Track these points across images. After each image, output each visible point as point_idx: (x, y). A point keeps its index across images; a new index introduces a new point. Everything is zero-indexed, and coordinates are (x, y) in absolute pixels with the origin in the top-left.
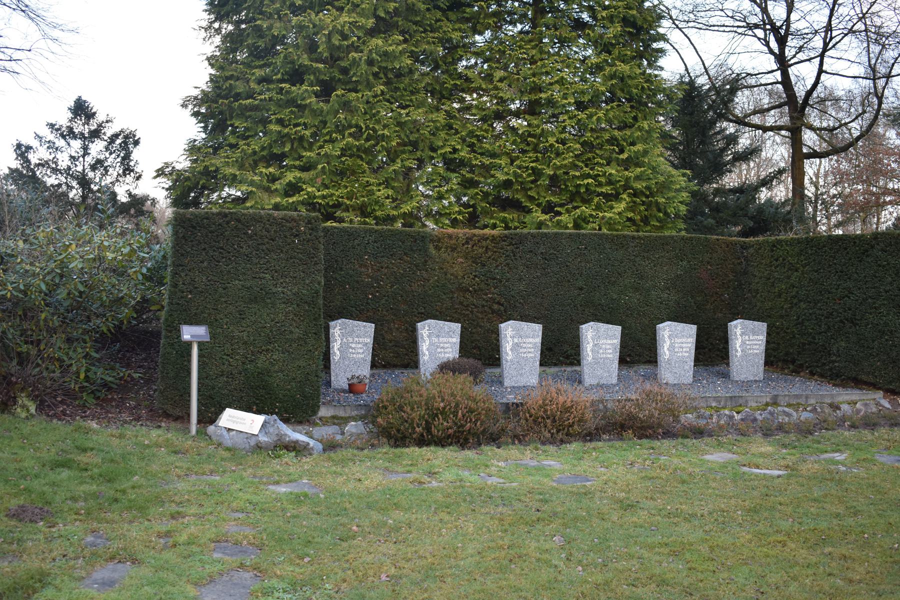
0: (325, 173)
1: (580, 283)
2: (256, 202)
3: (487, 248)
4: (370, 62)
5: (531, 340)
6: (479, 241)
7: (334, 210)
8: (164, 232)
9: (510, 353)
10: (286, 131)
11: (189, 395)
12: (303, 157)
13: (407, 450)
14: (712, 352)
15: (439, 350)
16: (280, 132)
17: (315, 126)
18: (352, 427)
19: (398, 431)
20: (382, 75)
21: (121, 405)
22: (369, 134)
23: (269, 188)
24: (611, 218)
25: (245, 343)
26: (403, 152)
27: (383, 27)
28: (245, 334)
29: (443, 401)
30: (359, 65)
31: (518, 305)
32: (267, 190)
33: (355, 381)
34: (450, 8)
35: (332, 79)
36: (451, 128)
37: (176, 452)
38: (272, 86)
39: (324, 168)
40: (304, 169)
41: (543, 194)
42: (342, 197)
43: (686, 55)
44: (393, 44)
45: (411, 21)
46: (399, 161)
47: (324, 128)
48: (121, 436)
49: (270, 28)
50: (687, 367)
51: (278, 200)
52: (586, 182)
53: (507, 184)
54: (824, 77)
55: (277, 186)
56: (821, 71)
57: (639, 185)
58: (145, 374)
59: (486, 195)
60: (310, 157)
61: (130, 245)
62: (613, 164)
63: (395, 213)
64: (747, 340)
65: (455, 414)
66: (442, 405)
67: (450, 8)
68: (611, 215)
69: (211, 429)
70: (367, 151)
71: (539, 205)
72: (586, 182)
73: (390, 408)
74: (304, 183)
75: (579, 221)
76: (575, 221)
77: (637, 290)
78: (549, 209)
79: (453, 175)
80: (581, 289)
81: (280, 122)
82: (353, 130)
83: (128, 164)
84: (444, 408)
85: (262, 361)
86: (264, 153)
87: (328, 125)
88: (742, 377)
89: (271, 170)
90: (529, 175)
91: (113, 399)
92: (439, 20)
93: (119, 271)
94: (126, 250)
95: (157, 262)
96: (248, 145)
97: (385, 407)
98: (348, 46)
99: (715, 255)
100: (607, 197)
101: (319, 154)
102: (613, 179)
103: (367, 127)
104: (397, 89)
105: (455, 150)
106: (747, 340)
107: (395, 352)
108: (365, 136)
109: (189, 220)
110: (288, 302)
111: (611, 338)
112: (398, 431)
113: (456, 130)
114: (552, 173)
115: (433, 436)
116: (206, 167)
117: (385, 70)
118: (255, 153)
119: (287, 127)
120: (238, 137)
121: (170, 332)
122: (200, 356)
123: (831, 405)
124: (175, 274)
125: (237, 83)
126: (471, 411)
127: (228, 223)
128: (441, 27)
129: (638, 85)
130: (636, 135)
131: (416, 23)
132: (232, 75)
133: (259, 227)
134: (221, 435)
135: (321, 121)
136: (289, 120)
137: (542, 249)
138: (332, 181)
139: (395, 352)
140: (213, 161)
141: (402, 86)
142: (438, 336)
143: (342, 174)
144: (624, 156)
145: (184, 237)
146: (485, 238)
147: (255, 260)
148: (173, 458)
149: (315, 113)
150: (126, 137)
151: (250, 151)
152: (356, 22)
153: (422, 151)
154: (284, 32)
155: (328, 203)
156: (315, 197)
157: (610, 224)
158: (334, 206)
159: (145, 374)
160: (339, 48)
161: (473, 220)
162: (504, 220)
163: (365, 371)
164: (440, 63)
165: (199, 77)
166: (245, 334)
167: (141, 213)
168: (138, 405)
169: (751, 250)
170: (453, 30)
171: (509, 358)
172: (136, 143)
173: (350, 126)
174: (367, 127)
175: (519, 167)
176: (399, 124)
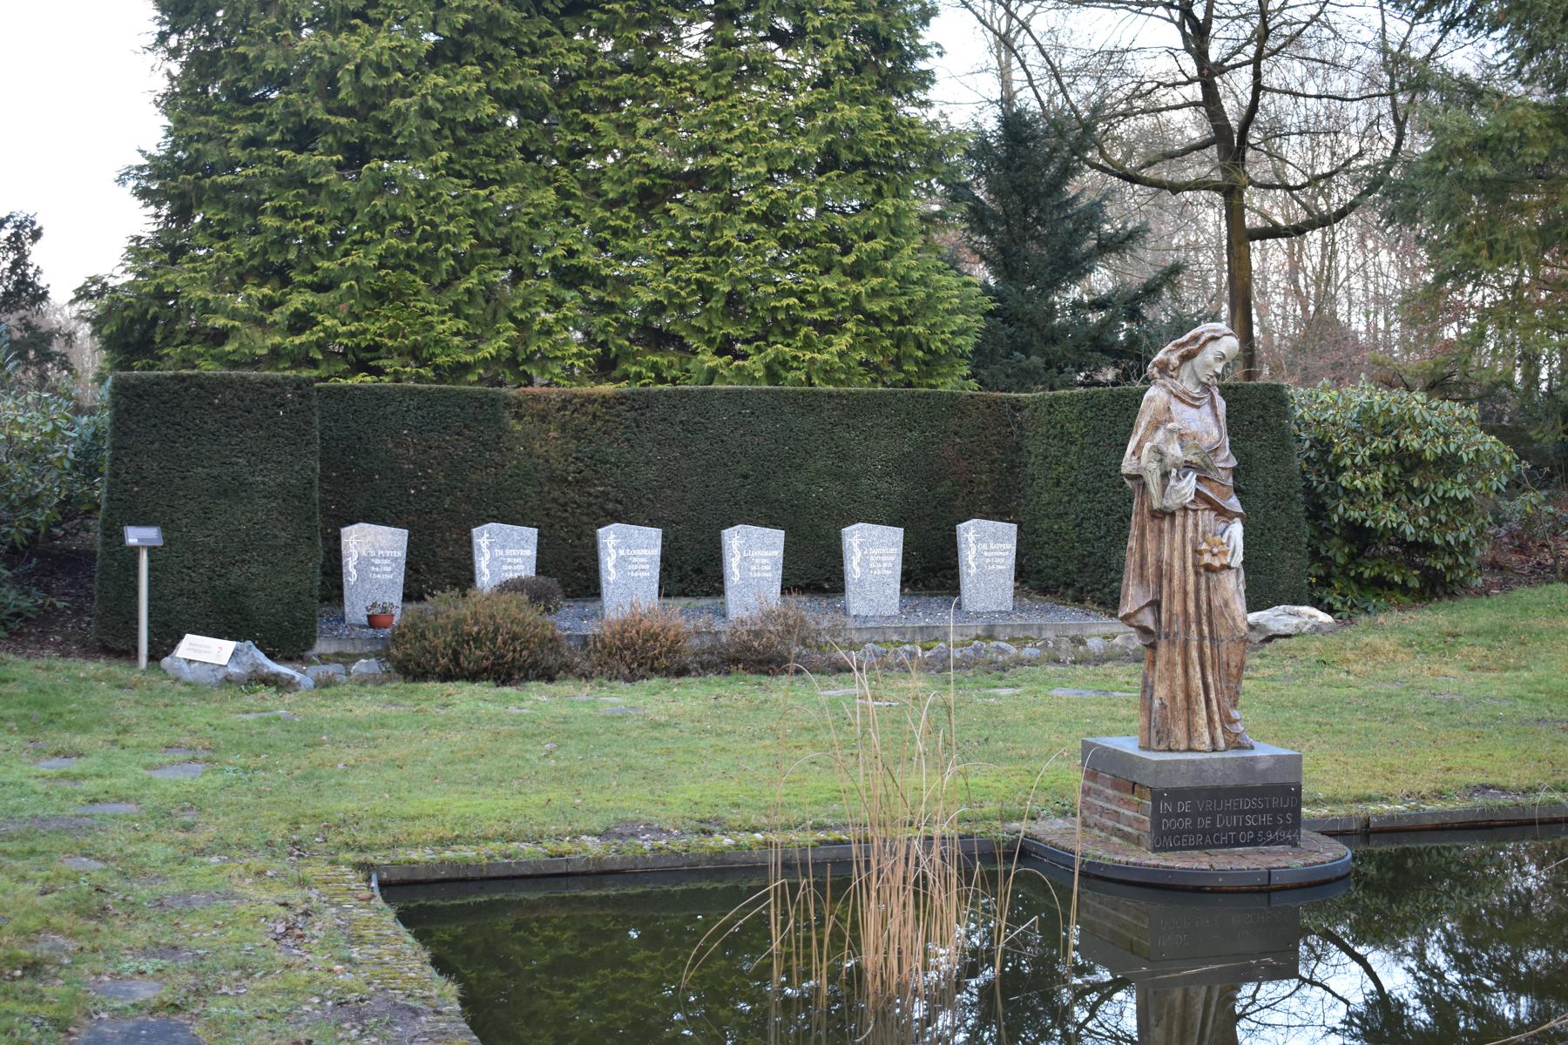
0: (353, 296)
1: (745, 468)
2: (242, 344)
3: (594, 416)
4: (426, 113)
5: (645, 552)
6: (582, 405)
7: (369, 355)
8: (95, 394)
9: (613, 571)
10: (289, 226)
11: (137, 621)
12: (317, 268)
13: (424, 685)
14: (930, 571)
15: (505, 567)
16: (279, 229)
17: (336, 218)
18: (361, 666)
19: (418, 665)
20: (447, 132)
21: (42, 642)
22: (424, 231)
23: (263, 319)
24: (826, 362)
25: (212, 552)
26: (484, 257)
27: (447, 54)
28: (212, 539)
29: (477, 622)
30: (405, 120)
31: (645, 502)
32: (260, 322)
33: (377, 611)
34: (565, 12)
35: (364, 140)
36: (568, 214)
37: (120, 687)
38: (265, 153)
39: (351, 287)
40: (319, 288)
41: (717, 323)
42: (381, 335)
43: (960, 90)
44: (467, 80)
45: (496, 39)
46: (474, 273)
47: (352, 221)
48: (48, 669)
49: (260, 58)
50: (888, 592)
51: (277, 339)
52: (785, 302)
53: (657, 308)
54: (1265, 100)
55: (277, 316)
56: (1258, 88)
57: (873, 307)
58: (72, 602)
59: (626, 326)
60: (328, 269)
61: (53, 420)
62: (836, 271)
63: (469, 358)
64: (986, 550)
65: (493, 640)
66: (476, 629)
67: (565, 12)
68: (826, 356)
69: (166, 661)
70: (421, 258)
71: (710, 342)
72: (785, 302)
73: (409, 636)
74: (320, 311)
75: (777, 367)
76: (768, 367)
77: (837, 477)
78: (724, 348)
79: (569, 295)
80: (746, 477)
81: (280, 212)
82: (399, 224)
83: (24, 275)
84: (478, 633)
85: (236, 576)
86: (255, 262)
87: (358, 216)
88: (979, 607)
89: (266, 290)
90: (693, 293)
91: (30, 634)
92: (548, 34)
93: (33, 455)
94: (48, 428)
95: (84, 443)
96: (228, 249)
97: (403, 635)
98: (389, 87)
99: (966, 421)
100: (823, 327)
101: (342, 264)
102: (833, 296)
103: (422, 221)
104: (473, 154)
105: (571, 253)
106: (986, 550)
107: (438, 566)
108: (417, 235)
109: (134, 386)
110: (270, 496)
111: (769, 547)
112: (418, 665)
113: (576, 217)
114: (727, 289)
115: (462, 669)
116: (159, 287)
117: (452, 124)
118: (239, 262)
119: (291, 219)
120: (211, 235)
121: (110, 537)
122: (150, 569)
123: (1073, 639)
124: (115, 460)
125: (208, 147)
126: (515, 638)
127: (186, 389)
128: (548, 46)
129: (875, 141)
130: (872, 223)
131: (505, 43)
132: (199, 134)
133: (228, 395)
134: (180, 669)
135: (348, 210)
136: (295, 209)
137: (682, 416)
138: (366, 308)
139: (438, 566)
140: (170, 277)
141: (481, 148)
142: (503, 547)
143: (380, 296)
144: (849, 260)
145: (126, 410)
146: (590, 399)
147: (224, 440)
148: (117, 692)
149: (336, 197)
150: (20, 226)
151: (231, 260)
152: (402, 46)
153: (518, 254)
154: (284, 66)
155: (358, 345)
156: (337, 335)
157: (828, 373)
158: (368, 349)
159: (72, 602)
160: (375, 89)
161: (605, 366)
162: (654, 367)
163: (395, 597)
164: (550, 105)
165: (151, 133)
166: (212, 539)
167: (46, 356)
168: (66, 639)
169: (1026, 413)
170: (569, 50)
171: (611, 579)
172: (36, 235)
173: (394, 218)
174: (422, 221)
175: (676, 280)
176: (475, 213)
